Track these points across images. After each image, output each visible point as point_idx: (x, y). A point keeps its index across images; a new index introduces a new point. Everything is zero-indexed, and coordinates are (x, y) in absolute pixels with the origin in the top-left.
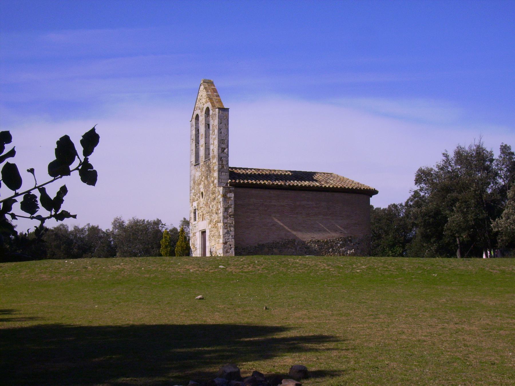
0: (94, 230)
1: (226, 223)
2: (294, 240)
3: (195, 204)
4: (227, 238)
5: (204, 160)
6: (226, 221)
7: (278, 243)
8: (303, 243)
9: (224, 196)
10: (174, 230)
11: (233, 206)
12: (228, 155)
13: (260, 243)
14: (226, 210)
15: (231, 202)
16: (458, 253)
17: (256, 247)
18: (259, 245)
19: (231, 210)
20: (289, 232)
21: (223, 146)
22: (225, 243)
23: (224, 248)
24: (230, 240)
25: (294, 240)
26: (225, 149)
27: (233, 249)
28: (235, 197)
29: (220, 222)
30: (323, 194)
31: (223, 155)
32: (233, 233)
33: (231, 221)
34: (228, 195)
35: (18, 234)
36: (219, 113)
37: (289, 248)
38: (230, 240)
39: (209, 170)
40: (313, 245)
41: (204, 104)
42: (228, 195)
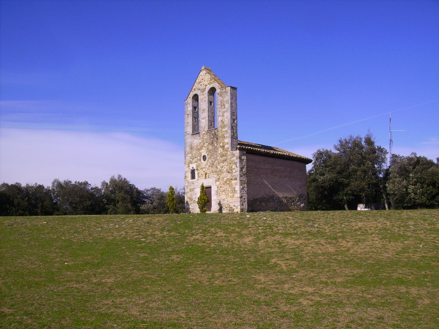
0: (41, 187)
1: (242, 180)
2: (274, 196)
3: (191, 166)
4: (242, 193)
5: (206, 129)
6: (241, 179)
7: (265, 198)
8: (279, 198)
9: (240, 158)
10: (96, 188)
11: (245, 167)
12: (237, 125)
13: (255, 198)
14: (241, 169)
15: (244, 163)
16: (346, 206)
17: (252, 201)
18: (254, 199)
19: (244, 170)
20: (271, 189)
21: (234, 118)
22: (241, 197)
23: (241, 201)
24: (244, 195)
25: (274, 196)
26: (235, 120)
27: (246, 202)
28: (246, 159)
29: (236, 179)
30: (289, 162)
31: (234, 125)
32: (246, 189)
33: (244, 179)
34: (243, 158)
35: (435, 161)
36: (231, 90)
37: (271, 202)
38: (244, 195)
39: (214, 136)
40: (284, 200)
41: (206, 86)
42: (243, 158)
